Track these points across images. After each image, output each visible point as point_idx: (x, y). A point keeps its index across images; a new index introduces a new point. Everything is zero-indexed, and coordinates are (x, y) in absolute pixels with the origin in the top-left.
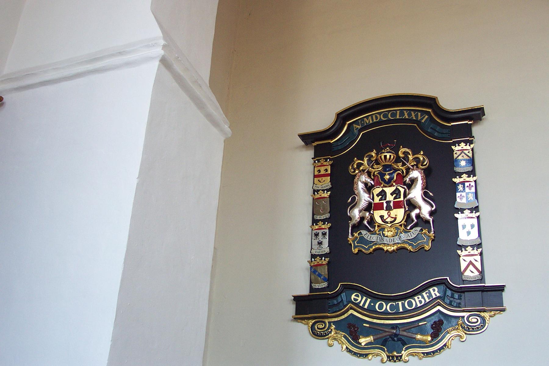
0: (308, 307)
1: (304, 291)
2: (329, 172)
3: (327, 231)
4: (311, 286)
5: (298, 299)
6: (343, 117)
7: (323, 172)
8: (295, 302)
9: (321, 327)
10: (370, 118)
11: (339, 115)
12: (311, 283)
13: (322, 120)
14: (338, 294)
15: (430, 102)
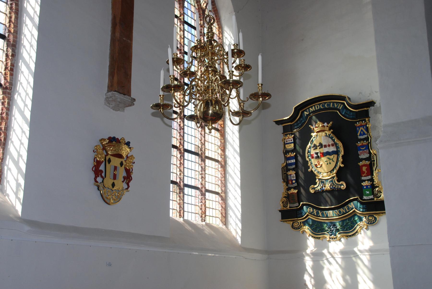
2: (293, 141)
3: (294, 175)
4: (285, 147)
6: (298, 109)
7: (290, 142)
9: (296, 224)
10: (313, 107)
12: (285, 144)
15: (342, 98)
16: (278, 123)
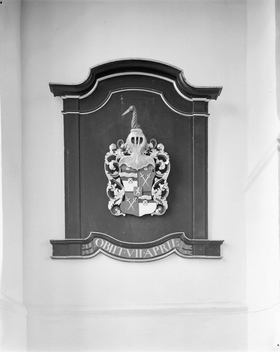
0: (60, 249)
1: (61, 236)
5: (55, 243)
6: (97, 72)
13: (80, 77)
15: (173, 73)
16: (57, 89)
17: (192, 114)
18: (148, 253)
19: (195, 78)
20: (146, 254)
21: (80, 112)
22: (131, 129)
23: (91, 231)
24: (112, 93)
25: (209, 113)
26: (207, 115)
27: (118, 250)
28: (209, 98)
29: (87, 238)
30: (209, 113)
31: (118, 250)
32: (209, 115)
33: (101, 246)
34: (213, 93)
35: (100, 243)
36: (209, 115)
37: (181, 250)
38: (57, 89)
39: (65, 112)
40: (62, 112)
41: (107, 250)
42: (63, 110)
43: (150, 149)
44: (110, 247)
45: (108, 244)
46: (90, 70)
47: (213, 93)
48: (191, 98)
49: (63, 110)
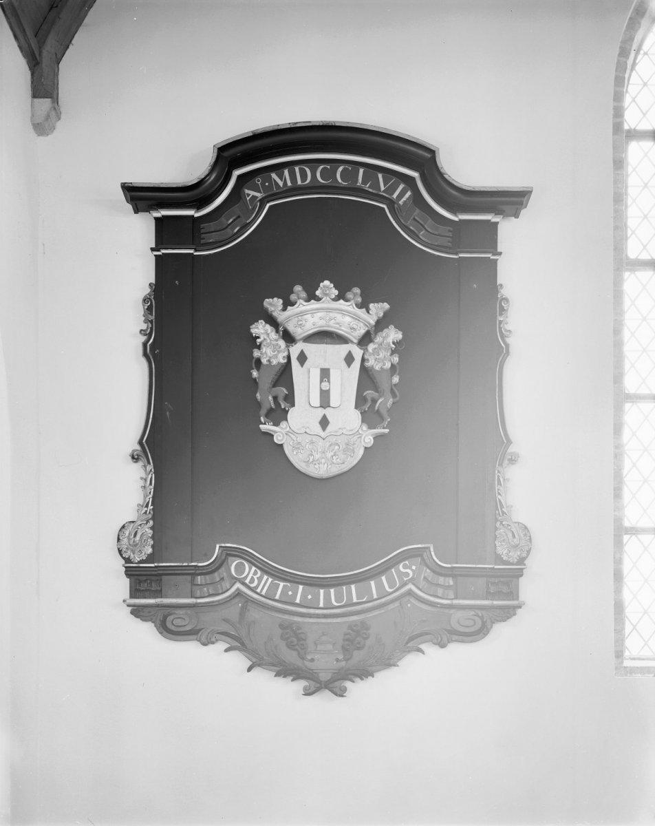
6: (232, 154)
8: (127, 581)
11: (222, 150)
13: (182, 160)
14: (221, 563)
15: (422, 158)
17: (456, 254)
18: (248, 195)
19: (466, 167)
20: (248, 199)
21: (196, 251)
22: (286, 342)
23: (219, 543)
24: (268, 205)
25: (499, 250)
26: (494, 255)
27: (274, 587)
28: (498, 212)
29: (215, 556)
30: (499, 250)
31: (274, 587)
32: (500, 254)
33: (243, 576)
34: (511, 201)
35: (240, 568)
36: (500, 254)
37: (422, 584)
38: (141, 197)
39: (158, 250)
40: (152, 250)
41: (252, 585)
42: (154, 246)
43: (637, 13)
44: (260, 579)
45: (255, 573)
46: (216, 151)
47: (511, 201)
48: (454, 212)
49: (154, 246)
